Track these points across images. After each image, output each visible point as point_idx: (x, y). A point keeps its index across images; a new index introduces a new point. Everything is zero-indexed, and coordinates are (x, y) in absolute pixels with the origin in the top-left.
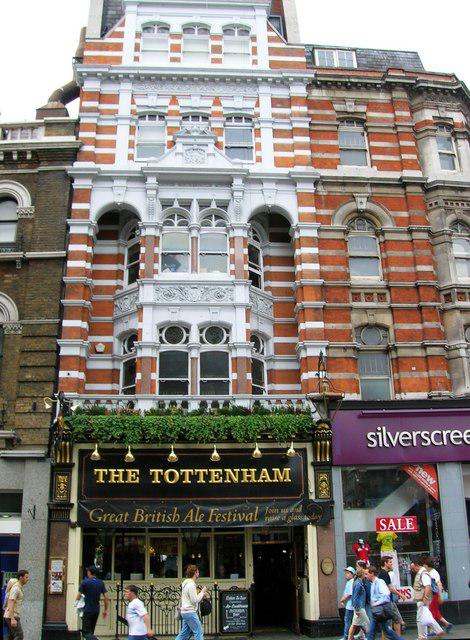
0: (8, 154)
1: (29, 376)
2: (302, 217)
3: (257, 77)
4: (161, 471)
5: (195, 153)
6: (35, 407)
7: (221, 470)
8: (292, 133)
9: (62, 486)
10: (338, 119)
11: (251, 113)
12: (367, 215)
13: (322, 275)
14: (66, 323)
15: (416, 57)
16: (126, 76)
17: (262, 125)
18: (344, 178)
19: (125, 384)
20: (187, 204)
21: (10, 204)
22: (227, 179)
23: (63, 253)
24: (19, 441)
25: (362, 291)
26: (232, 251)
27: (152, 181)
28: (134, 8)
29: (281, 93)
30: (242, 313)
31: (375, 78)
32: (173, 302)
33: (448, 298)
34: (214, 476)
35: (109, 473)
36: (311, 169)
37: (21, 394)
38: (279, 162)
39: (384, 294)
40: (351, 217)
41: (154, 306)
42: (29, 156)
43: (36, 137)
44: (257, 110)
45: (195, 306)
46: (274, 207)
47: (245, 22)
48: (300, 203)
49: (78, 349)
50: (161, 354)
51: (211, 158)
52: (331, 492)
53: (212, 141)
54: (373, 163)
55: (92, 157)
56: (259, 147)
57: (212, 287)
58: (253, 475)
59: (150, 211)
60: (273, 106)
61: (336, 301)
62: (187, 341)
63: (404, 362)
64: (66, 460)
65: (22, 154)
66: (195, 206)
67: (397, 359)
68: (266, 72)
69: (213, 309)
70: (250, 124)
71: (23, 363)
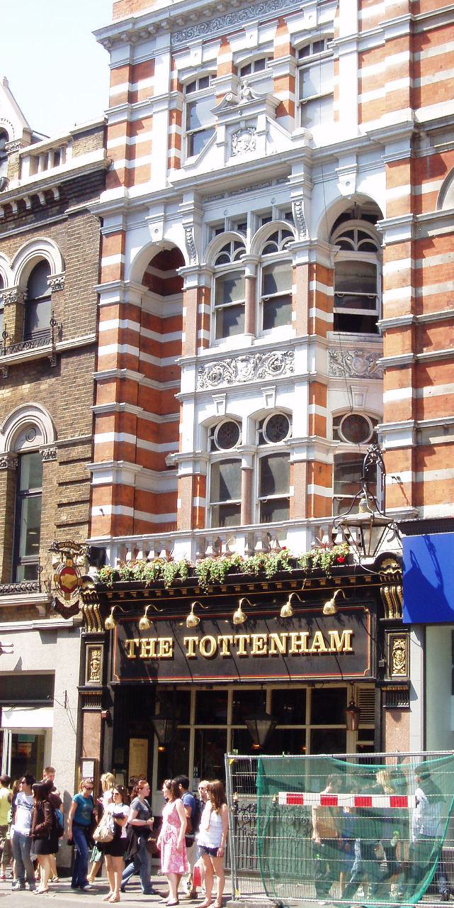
0: (7, 207)
4: (196, 638)
7: (264, 636)
16: (158, 27)
22: (279, 170)
23: (91, 337)
30: (302, 391)
34: (255, 643)
35: (251, 639)
50: (336, 457)
52: (407, 668)
58: (303, 642)
65: (48, 193)
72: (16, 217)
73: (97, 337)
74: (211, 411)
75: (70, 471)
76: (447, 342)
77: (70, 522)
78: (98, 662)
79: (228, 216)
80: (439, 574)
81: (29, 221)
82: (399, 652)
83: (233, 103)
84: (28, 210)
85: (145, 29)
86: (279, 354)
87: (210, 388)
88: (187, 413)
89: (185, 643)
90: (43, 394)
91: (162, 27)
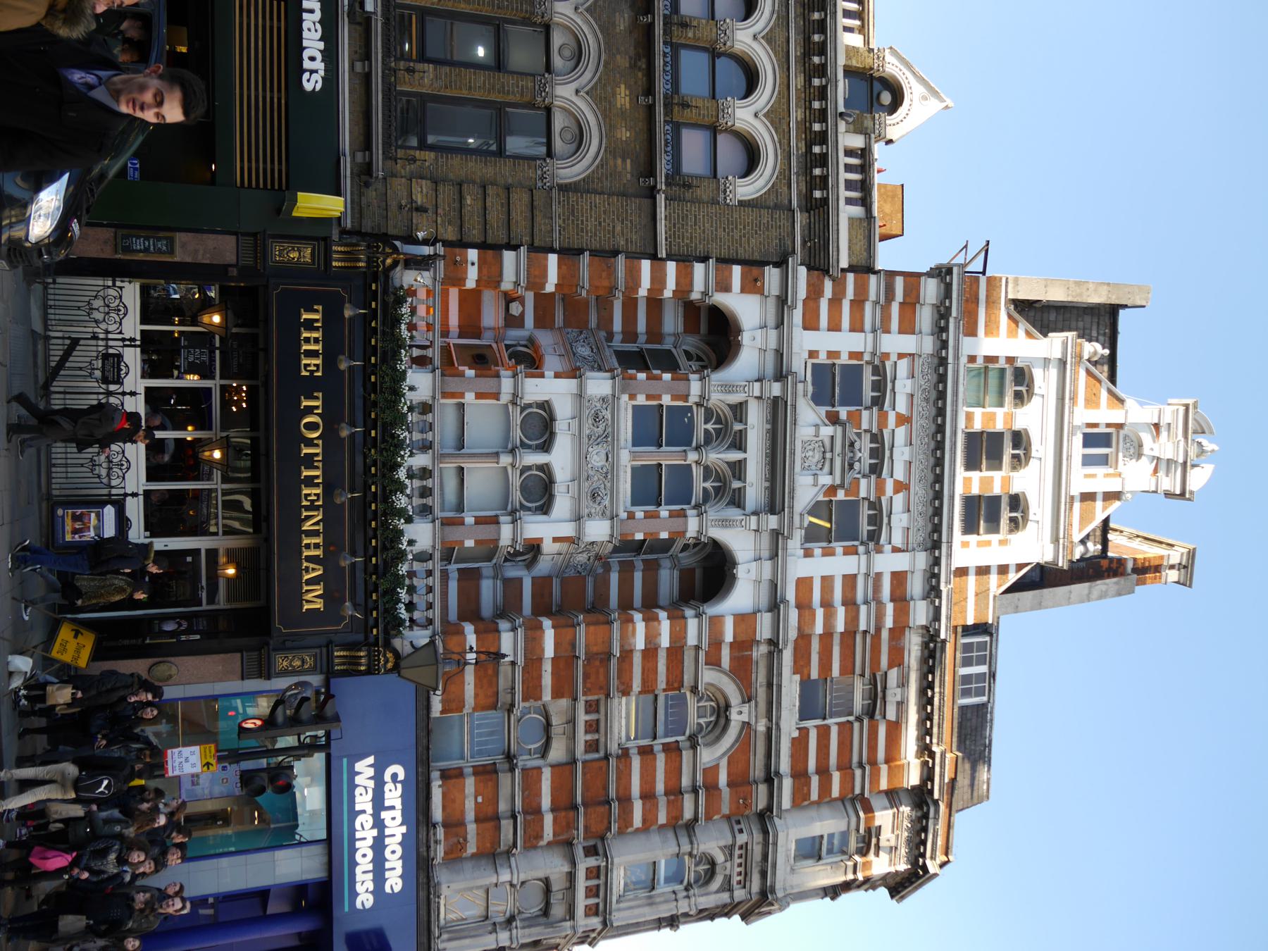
2: (716, 621)
3: (940, 548)
5: (818, 456)
12: (722, 721)
13: (627, 654)
18: (780, 687)
20: (739, 443)
24: (367, 185)
27: (776, 389)
29: (916, 586)
36: (793, 634)
38: (804, 584)
41: (580, 396)
42: (817, 194)
45: (581, 457)
52: (285, 673)
53: (838, 482)
54: (804, 732)
55: (814, 293)
61: (586, 676)
66: (735, 456)
68: (949, 555)
72: (808, 124)
73: (661, 259)
74: (563, 410)
75: (521, 212)
79: (747, 488)
81: (800, 145)
83: (851, 466)
84: (812, 194)
85: (945, 329)
86: (607, 502)
88: (569, 385)
89: (315, 307)
90: (611, 163)
91: (941, 349)
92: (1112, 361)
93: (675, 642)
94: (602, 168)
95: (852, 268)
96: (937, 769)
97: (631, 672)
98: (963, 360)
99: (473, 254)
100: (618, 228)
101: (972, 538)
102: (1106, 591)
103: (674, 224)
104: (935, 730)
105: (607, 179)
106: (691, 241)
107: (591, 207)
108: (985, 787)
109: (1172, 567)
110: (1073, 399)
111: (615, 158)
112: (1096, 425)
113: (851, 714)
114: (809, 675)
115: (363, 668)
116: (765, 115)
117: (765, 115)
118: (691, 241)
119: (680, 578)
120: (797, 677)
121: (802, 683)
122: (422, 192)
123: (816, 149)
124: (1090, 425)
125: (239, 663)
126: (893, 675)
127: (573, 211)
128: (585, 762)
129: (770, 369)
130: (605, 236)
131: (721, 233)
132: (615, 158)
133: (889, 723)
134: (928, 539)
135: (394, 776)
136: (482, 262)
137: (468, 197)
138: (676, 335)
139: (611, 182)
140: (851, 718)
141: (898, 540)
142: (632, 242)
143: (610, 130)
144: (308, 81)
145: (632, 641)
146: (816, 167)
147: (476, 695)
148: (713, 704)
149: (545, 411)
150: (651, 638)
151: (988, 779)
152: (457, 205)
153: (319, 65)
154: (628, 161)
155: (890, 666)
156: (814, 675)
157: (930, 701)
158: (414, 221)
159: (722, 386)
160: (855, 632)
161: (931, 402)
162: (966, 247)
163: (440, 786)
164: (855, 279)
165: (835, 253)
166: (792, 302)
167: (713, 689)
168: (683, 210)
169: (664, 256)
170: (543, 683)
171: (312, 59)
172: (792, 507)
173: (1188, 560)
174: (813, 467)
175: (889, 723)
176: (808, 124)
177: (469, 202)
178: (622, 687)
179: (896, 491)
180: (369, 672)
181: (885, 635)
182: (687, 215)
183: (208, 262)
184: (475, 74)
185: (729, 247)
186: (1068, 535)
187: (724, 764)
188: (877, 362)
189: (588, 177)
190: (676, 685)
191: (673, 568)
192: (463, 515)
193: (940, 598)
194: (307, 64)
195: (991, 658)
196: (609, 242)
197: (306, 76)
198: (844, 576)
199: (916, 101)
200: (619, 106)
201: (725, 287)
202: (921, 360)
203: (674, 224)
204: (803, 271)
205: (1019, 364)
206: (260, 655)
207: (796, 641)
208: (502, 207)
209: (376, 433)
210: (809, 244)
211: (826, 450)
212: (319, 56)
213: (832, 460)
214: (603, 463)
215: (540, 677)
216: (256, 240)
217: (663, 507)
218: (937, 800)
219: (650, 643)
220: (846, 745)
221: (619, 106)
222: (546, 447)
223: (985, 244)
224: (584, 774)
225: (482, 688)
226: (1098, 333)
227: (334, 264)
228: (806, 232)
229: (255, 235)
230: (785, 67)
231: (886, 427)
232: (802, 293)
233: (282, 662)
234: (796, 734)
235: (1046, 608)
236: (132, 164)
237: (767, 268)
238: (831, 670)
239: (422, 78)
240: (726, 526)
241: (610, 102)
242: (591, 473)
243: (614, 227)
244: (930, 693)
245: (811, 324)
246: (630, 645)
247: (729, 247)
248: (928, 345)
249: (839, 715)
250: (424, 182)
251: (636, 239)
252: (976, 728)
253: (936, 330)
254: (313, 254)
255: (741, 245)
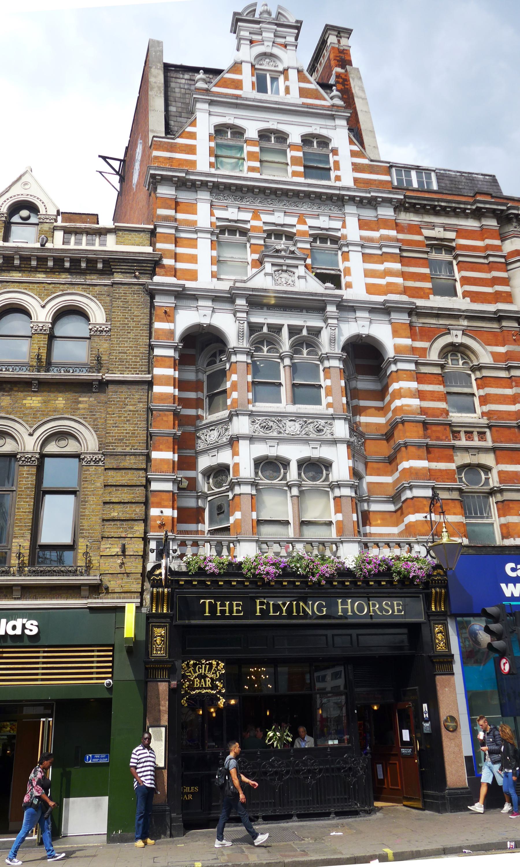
1: (115, 514)
2: (397, 348)
3: (344, 195)
5: (284, 275)
6: (124, 550)
8: (384, 258)
9: (440, 636)
10: (427, 246)
11: (339, 234)
12: (462, 349)
13: (423, 411)
14: (155, 455)
15: (493, 180)
17: (351, 248)
18: (440, 309)
19: (212, 521)
20: (277, 329)
21: (25, 317)
23: (148, 377)
24: (107, 589)
25: (463, 429)
26: (328, 382)
27: (241, 302)
28: (206, 106)
29: (368, 214)
30: (343, 449)
31: (465, 203)
32: (271, 434)
33: (456, 435)
36: (405, 298)
37: (106, 534)
38: (371, 289)
39: (484, 433)
40: (445, 350)
41: (252, 439)
42: (100, 266)
43: (105, 245)
44: (343, 231)
45: (293, 440)
46: (368, 336)
47: (324, 132)
48: (396, 333)
49: (249, 487)
51: (302, 281)
52: (448, 644)
53: (302, 262)
54: (465, 294)
55: (174, 272)
56: (347, 271)
57: (311, 420)
59: (240, 335)
60: (361, 228)
61: (438, 439)
62: (284, 478)
63: (511, 506)
64: (163, 610)
66: (285, 332)
67: (503, 502)
68: (348, 189)
69: (313, 444)
70: (336, 246)
71: (107, 499)
72: (48, 270)
73: (152, 377)
75: (122, 476)
76: (444, 438)
77: (123, 518)
78: (163, 639)
80: (76, 857)
82: (440, 635)
85: (194, 182)
86: (322, 422)
87: (261, 434)
90: (82, 411)
92: (207, 71)
93: (414, 378)
94: (87, 418)
95: (152, 244)
96: (488, 206)
97: (434, 408)
98: (213, 171)
99: (154, 512)
100: (131, 408)
101: (333, 174)
102: (359, 87)
103: (126, 368)
104: (462, 206)
105: (94, 415)
106: (138, 356)
107: (116, 427)
108: (487, 177)
109: (339, 41)
110: (237, 97)
111: (78, 409)
112: (253, 83)
113: (451, 263)
114: (430, 289)
115: (443, 591)
116: (43, 301)
117: (43, 301)
118: (138, 356)
119: (363, 374)
120: (431, 296)
121: (435, 294)
122: (110, 548)
123: (67, 265)
124: (253, 88)
125: (443, 677)
126: (427, 233)
127: (119, 440)
128: (494, 441)
129: (228, 306)
130: (137, 418)
131: (131, 335)
132: (78, 409)
133: (458, 237)
134: (336, 204)
135: (513, 570)
136: (159, 505)
137: (112, 514)
138: (197, 371)
139: (97, 412)
140: (455, 263)
141: (337, 224)
142: (140, 399)
143: (58, 411)
144: (31, 630)
145: (414, 407)
146: (80, 266)
147: (455, 514)
148: (449, 355)
149: (261, 463)
150: (412, 394)
151: (482, 175)
152: (118, 523)
153: (19, 623)
154: (80, 399)
155: (421, 234)
156: (429, 285)
157: (444, 208)
158: (131, 554)
159: (239, 339)
160: (401, 256)
161: (244, 195)
162: (100, 172)
163: (514, 539)
164: (161, 242)
165: (144, 255)
166: (180, 287)
167: (442, 354)
168: (116, 362)
169: (150, 376)
170: (444, 468)
171: (14, 628)
172: (322, 295)
173: (334, 30)
174: (293, 279)
175: (458, 237)
176: (48, 270)
177: (116, 514)
178: (444, 415)
179: (305, 223)
180: (446, 587)
181: (401, 236)
182: (120, 359)
183: (167, 703)
184: (18, 509)
185: (141, 330)
186: (329, 108)
187: (490, 348)
188: (217, 231)
189: (93, 428)
190: (441, 379)
191: (356, 379)
192: (334, 522)
193: (377, 197)
194: (18, 632)
195: (407, 168)
196: (141, 415)
197: (27, 632)
198: (364, 262)
199: (27, 192)
200: (39, 405)
201: (172, 333)
202: (214, 200)
203: (126, 368)
204: (157, 279)
205: (213, 132)
206: (437, 663)
207: (410, 296)
208: (119, 490)
209: (384, 581)
210: (137, 273)
211: (280, 268)
212: (12, 623)
213: (288, 266)
214: (215, 431)
215: (440, 471)
216: (150, 668)
217: (322, 383)
218: (507, 207)
219: (414, 395)
220: (474, 267)
221: (39, 405)
222: (285, 463)
223: (101, 159)
224: (501, 442)
225: (449, 510)
226: (182, 79)
227: (165, 611)
228: (128, 275)
229: (146, 669)
230: (5, 284)
231: (262, 227)
232: (172, 280)
233: (441, 647)
234: (468, 299)
235: (373, 128)
236: (89, 760)
237: (156, 304)
238: (425, 274)
239: (23, 547)
240: (330, 340)
241: (37, 411)
242: (303, 432)
243: (130, 411)
244: (438, 208)
245: (193, 275)
246: (417, 408)
247: (141, 330)
248: (204, 196)
249: (452, 271)
250: (102, 546)
251: (138, 394)
252: (451, 181)
253: (193, 189)
254: (159, 627)
255: (140, 322)
